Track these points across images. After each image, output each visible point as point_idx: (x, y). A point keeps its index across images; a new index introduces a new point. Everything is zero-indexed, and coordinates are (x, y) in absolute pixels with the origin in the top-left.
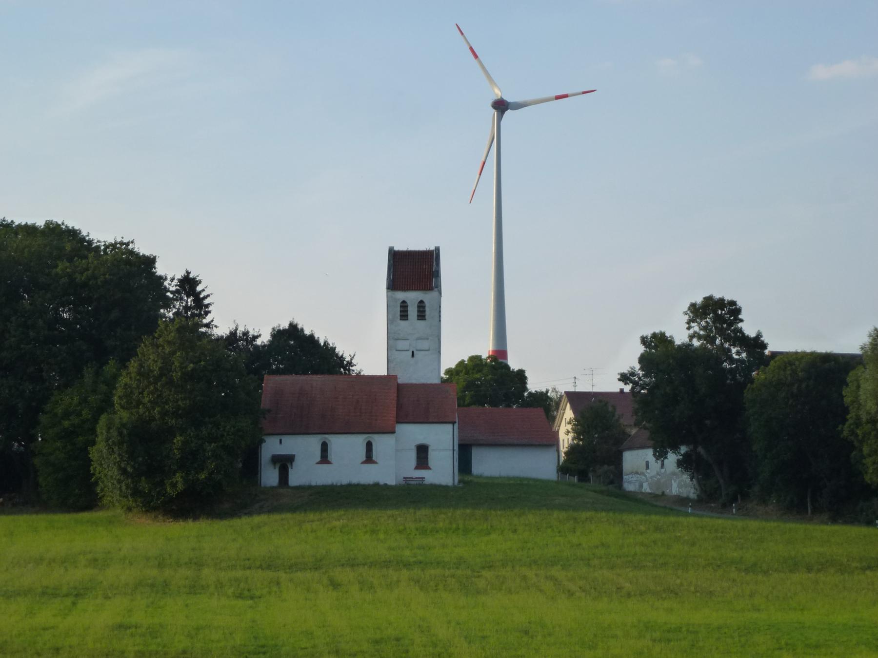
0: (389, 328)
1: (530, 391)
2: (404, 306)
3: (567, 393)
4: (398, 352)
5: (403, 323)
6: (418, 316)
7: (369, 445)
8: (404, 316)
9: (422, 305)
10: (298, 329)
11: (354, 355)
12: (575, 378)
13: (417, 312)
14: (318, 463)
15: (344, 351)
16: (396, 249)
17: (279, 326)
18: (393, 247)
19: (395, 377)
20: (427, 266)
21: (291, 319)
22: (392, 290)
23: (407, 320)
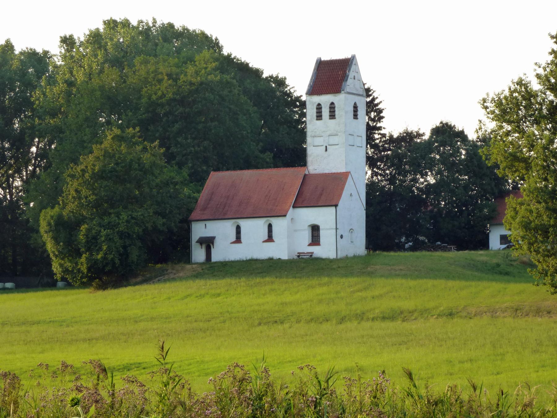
5: (319, 122)
9: (332, 106)
14: (264, 242)
23: (321, 119)
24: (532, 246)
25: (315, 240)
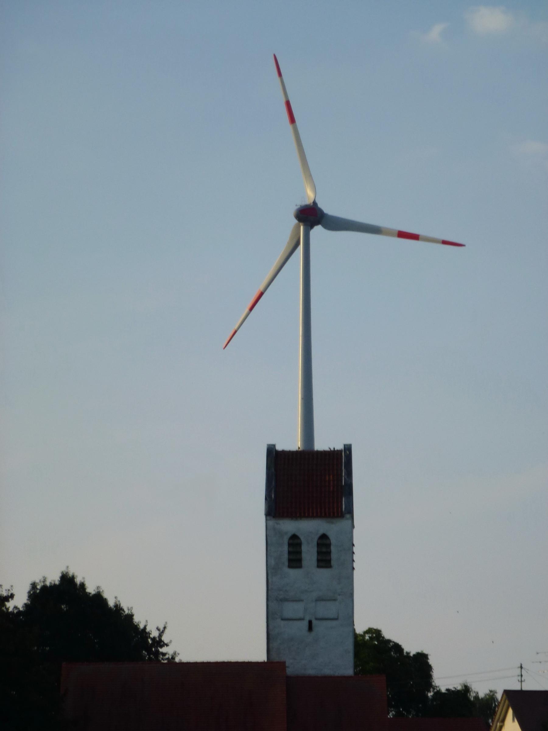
0: (270, 581)
3: (508, 693)
4: (286, 622)
5: (293, 573)
6: (318, 561)
10: (76, 584)
11: (165, 628)
12: (521, 667)
13: (315, 554)
15: (147, 621)
16: (279, 448)
17: (44, 581)
18: (274, 446)
19: (282, 665)
20: (327, 478)
21: (64, 569)
22: (274, 517)
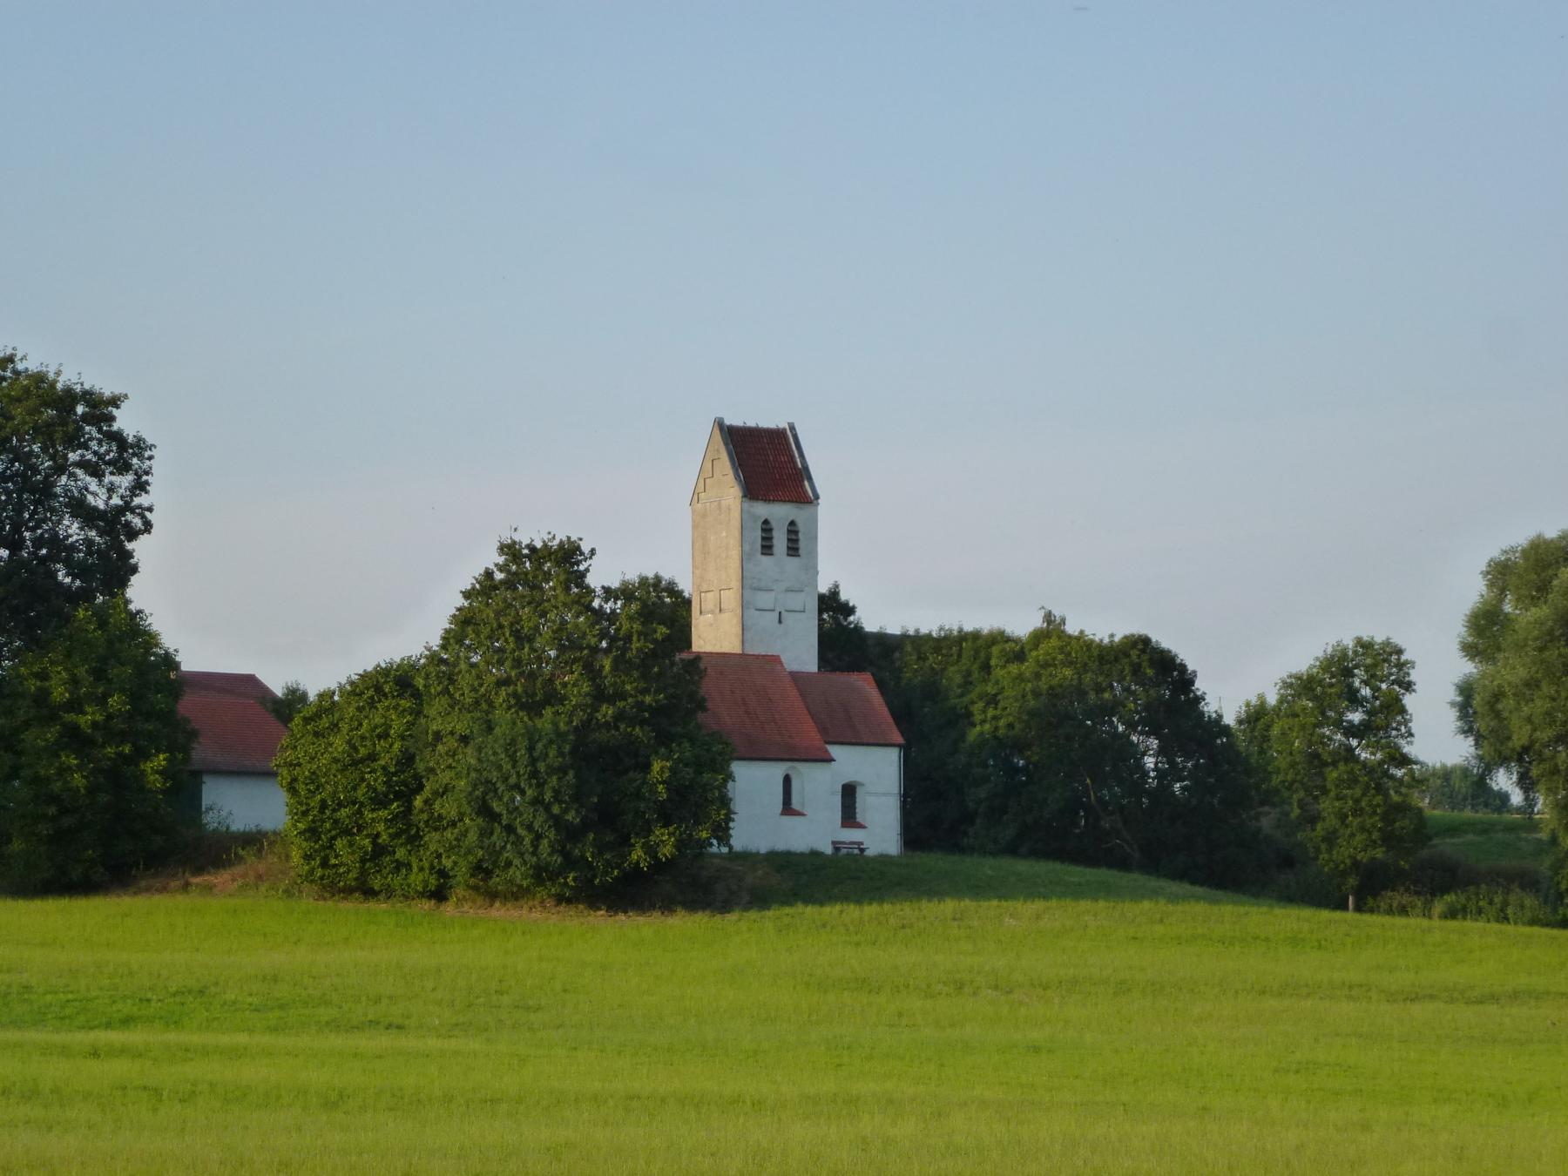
1: (1520, 548)
2: (767, 527)
5: (765, 559)
7: (787, 781)
8: (767, 549)
9: (792, 528)
22: (750, 499)
24: (496, 825)
25: (849, 817)
